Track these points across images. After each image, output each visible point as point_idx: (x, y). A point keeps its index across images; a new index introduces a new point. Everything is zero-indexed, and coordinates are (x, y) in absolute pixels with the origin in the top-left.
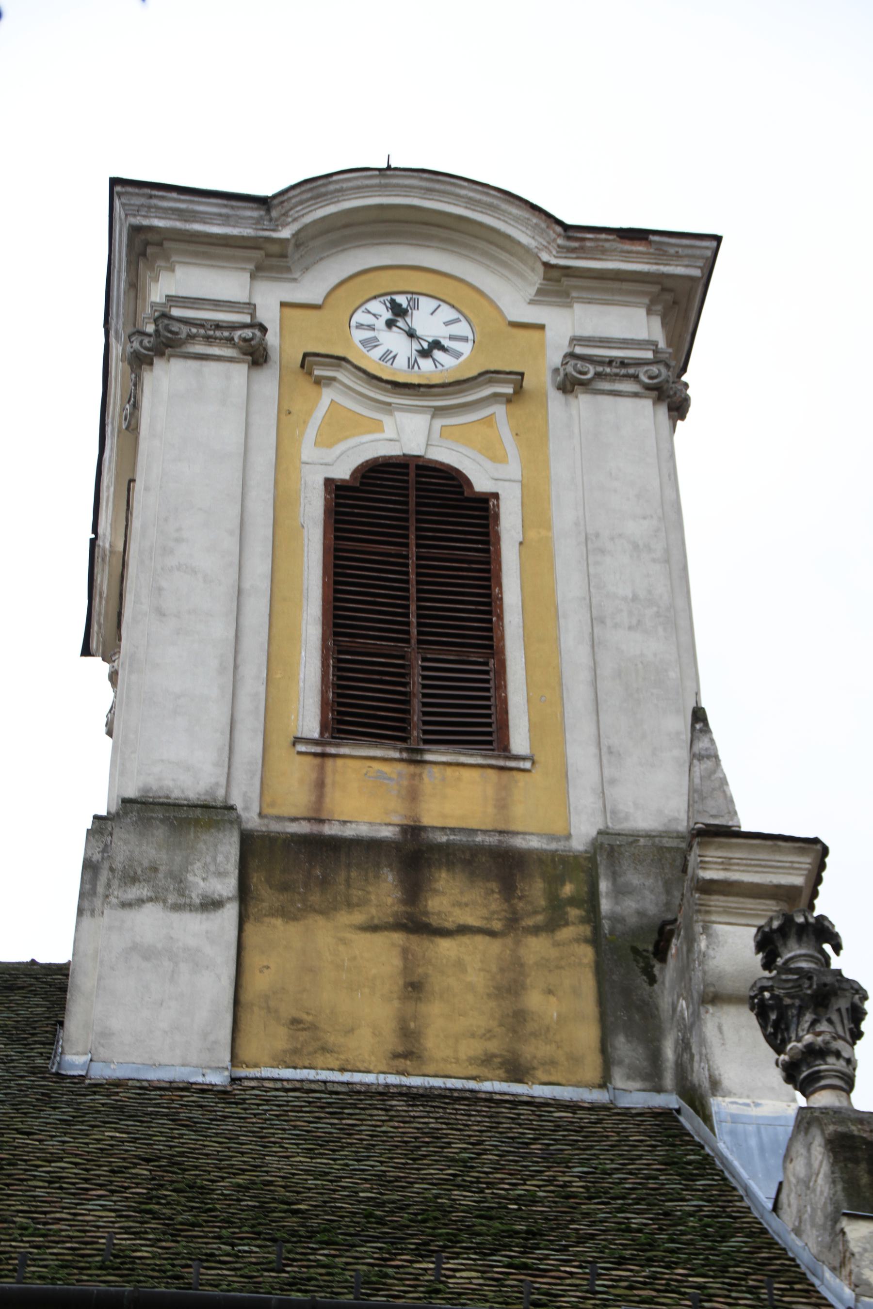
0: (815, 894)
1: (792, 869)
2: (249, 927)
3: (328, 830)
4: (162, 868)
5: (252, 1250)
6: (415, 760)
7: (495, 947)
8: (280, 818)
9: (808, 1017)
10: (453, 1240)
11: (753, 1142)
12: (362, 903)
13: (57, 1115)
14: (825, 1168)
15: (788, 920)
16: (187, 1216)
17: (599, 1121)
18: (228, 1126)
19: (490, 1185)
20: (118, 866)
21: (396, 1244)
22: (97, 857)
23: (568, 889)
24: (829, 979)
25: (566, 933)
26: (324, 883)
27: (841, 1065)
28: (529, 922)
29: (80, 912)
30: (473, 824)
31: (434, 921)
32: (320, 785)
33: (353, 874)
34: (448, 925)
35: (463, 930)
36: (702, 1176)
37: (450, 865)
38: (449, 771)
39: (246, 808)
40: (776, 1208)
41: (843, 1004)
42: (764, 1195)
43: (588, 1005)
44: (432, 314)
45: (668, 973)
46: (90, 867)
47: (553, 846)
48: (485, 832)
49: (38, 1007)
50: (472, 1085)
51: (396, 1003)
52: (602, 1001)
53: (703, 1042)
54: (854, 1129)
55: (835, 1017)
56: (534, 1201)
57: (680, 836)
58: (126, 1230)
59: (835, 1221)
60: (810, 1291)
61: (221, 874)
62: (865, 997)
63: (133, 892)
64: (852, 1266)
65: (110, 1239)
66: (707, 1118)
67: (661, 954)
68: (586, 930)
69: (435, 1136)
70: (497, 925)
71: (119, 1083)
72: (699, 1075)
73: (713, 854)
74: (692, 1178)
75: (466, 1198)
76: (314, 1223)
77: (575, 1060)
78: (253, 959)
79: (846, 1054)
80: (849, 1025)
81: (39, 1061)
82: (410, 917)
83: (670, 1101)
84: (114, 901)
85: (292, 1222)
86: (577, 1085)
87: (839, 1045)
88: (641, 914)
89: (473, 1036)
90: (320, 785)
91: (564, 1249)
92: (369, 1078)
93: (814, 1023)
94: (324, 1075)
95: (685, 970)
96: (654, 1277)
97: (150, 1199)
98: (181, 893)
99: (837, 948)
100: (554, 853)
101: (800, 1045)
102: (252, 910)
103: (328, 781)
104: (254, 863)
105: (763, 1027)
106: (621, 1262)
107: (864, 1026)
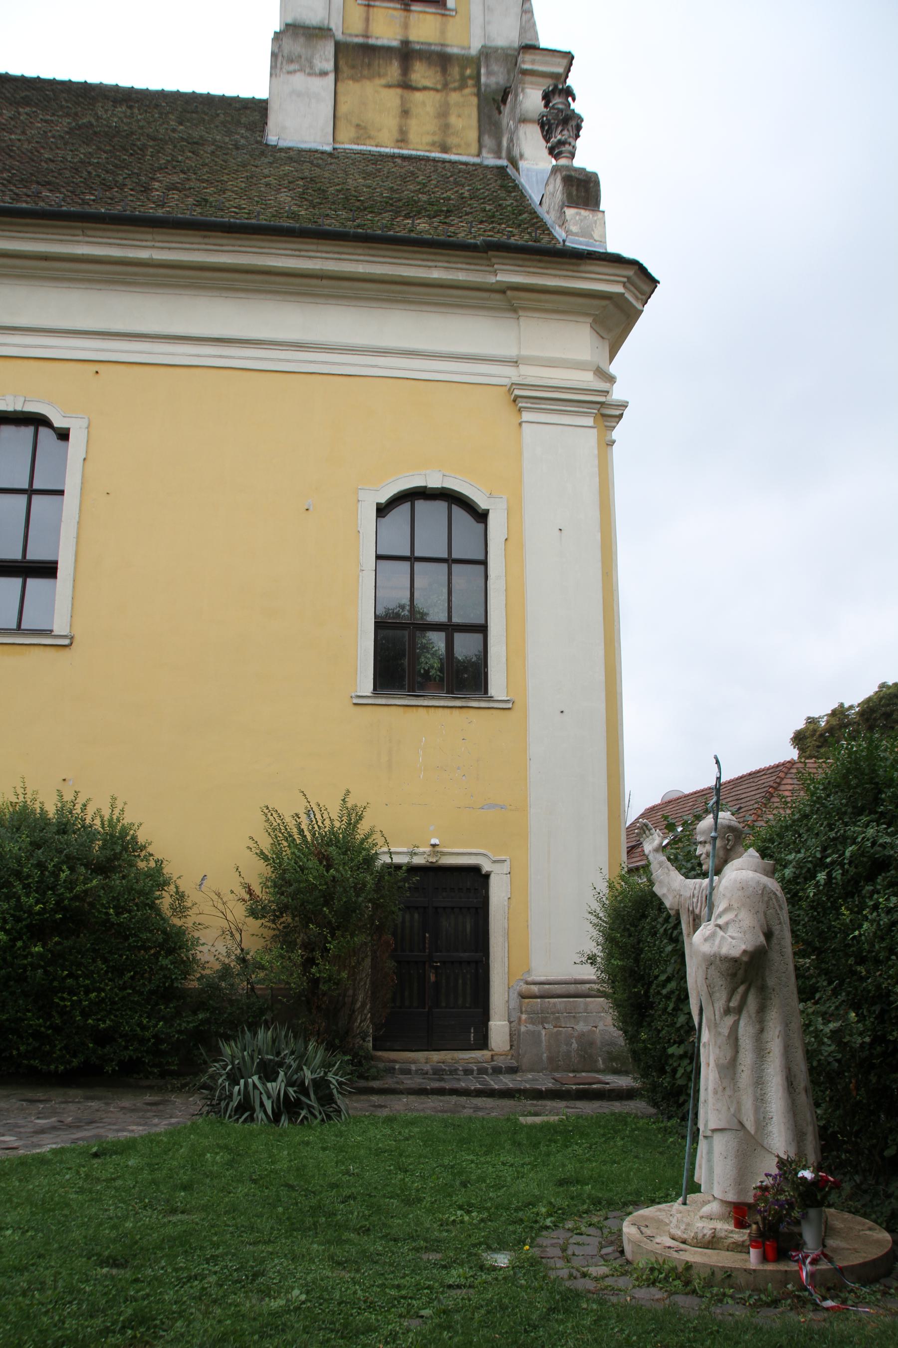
0: (567, 77)
1: (559, 65)
2: (339, 84)
3: (371, 41)
4: (303, 57)
5: (343, 214)
6: (407, 9)
7: (438, 96)
8: (350, 35)
9: (560, 128)
10: (419, 213)
11: (534, 179)
12: (385, 75)
13: (267, 160)
14: (561, 188)
15: (556, 87)
16: (318, 200)
17: (476, 170)
18: (333, 167)
19: (433, 193)
20: (285, 54)
21: (397, 213)
22: (276, 50)
23: (468, 72)
24: (569, 113)
25: (467, 91)
26: (369, 65)
27: (570, 148)
28: (452, 86)
29: (271, 75)
30: (431, 40)
31: (414, 84)
32: (367, 20)
33: (381, 62)
34: (420, 85)
35: (425, 88)
36: (514, 192)
37: (421, 59)
38: (421, 15)
39: (337, 30)
40: (540, 204)
41: (574, 123)
42: (537, 200)
43: (474, 122)
44: (716, 758)
45: (506, 110)
46: (274, 55)
47: (463, 52)
48: (435, 45)
49: (256, 116)
50: (427, 154)
51: (398, 119)
52: (479, 121)
53: (518, 139)
54: (573, 174)
55: (570, 129)
56: (450, 199)
57: (515, 49)
58: (296, 204)
59: (562, 208)
60: (550, 234)
61: (327, 60)
62: (582, 121)
63: (293, 67)
64: (566, 225)
65: (290, 207)
66: (517, 169)
67: (504, 101)
68: (475, 90)
69: (413, 173)
70: (439, 87)
71: (290, 149)
72: (516, 152)
73: (528, 57)
74: (510, 192)
75: (424, 198)
76: (366, 205)
77: (468, 145)
78: (341, 99)
79: (573, 144)
80: (575, 132)
81: (259, 139)
82: (404, 82)
83: (504, 162)
84: (284, 70)
85: (358, 204)
86: (468, 155)
87: (571, 140)
88: (497, 83)
89: (428, 133)
90: (367, 20)
91: (461, 217)
92: (387, 150)
93: (562, 131)
94: (369, 148)
95: (513, 109)
96: (494, 228)
97: (304, 193)
98: (311, 67)
99: (574, 100)
100: (463, 56)
101: (556, 140)
102: (340, 77)
103: (371, 18)
104: (340, 56)
105: (542, 132)
106: (481, 222)
107: (581, 133)
